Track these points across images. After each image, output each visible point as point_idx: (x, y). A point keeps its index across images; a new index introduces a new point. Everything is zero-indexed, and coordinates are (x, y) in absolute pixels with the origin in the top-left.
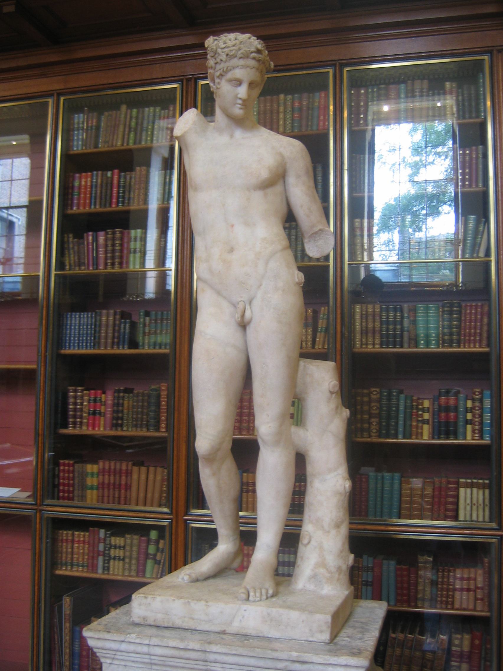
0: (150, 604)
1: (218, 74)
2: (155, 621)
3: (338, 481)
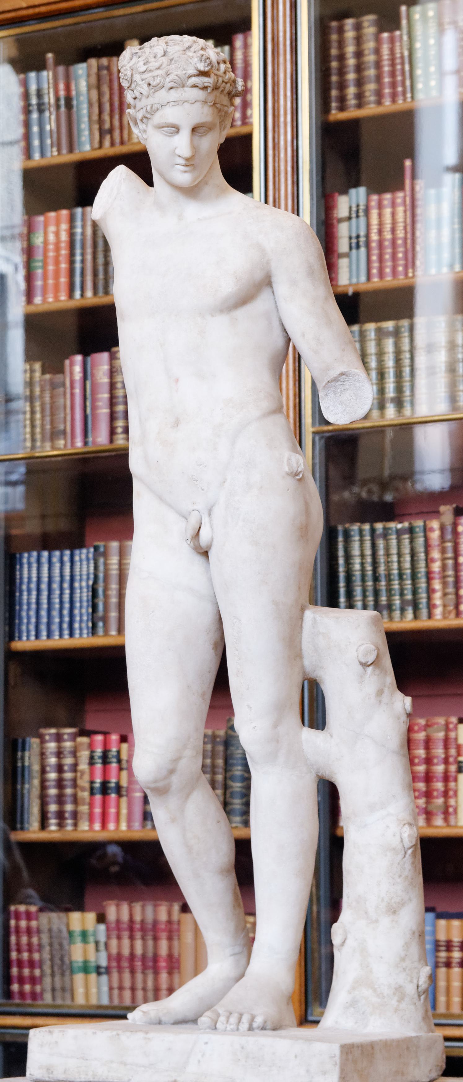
0: (56, 1042)
1: (139, 115)
2: (65, 1072)
3: (387, 827)
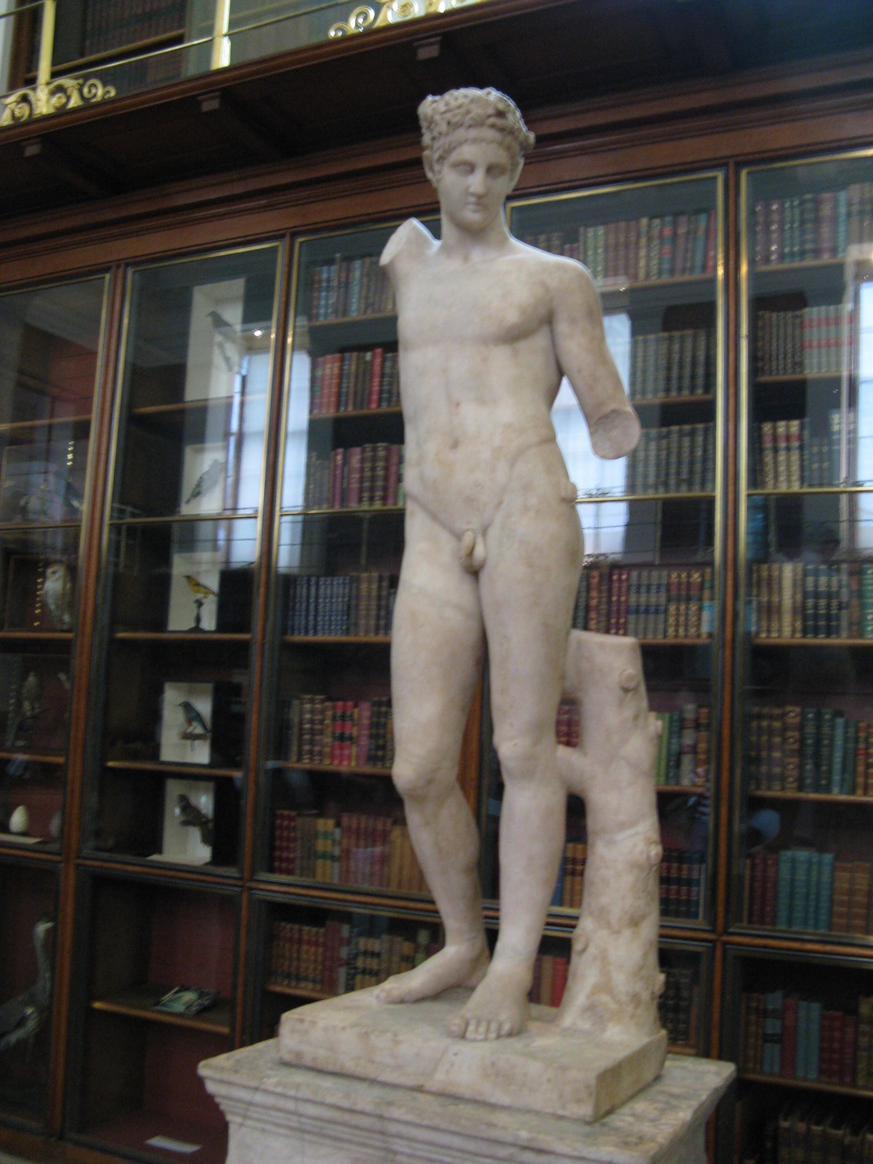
1: (436, 156)
